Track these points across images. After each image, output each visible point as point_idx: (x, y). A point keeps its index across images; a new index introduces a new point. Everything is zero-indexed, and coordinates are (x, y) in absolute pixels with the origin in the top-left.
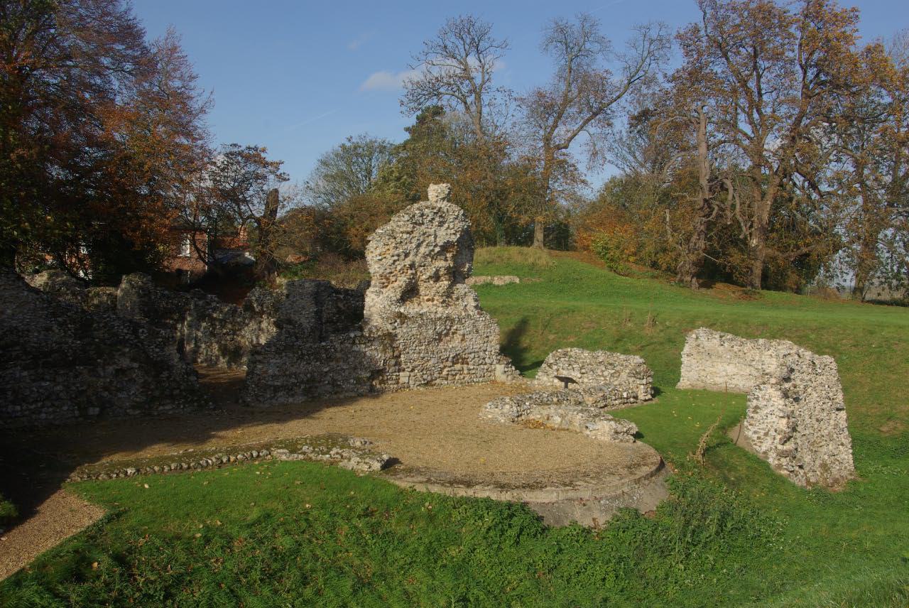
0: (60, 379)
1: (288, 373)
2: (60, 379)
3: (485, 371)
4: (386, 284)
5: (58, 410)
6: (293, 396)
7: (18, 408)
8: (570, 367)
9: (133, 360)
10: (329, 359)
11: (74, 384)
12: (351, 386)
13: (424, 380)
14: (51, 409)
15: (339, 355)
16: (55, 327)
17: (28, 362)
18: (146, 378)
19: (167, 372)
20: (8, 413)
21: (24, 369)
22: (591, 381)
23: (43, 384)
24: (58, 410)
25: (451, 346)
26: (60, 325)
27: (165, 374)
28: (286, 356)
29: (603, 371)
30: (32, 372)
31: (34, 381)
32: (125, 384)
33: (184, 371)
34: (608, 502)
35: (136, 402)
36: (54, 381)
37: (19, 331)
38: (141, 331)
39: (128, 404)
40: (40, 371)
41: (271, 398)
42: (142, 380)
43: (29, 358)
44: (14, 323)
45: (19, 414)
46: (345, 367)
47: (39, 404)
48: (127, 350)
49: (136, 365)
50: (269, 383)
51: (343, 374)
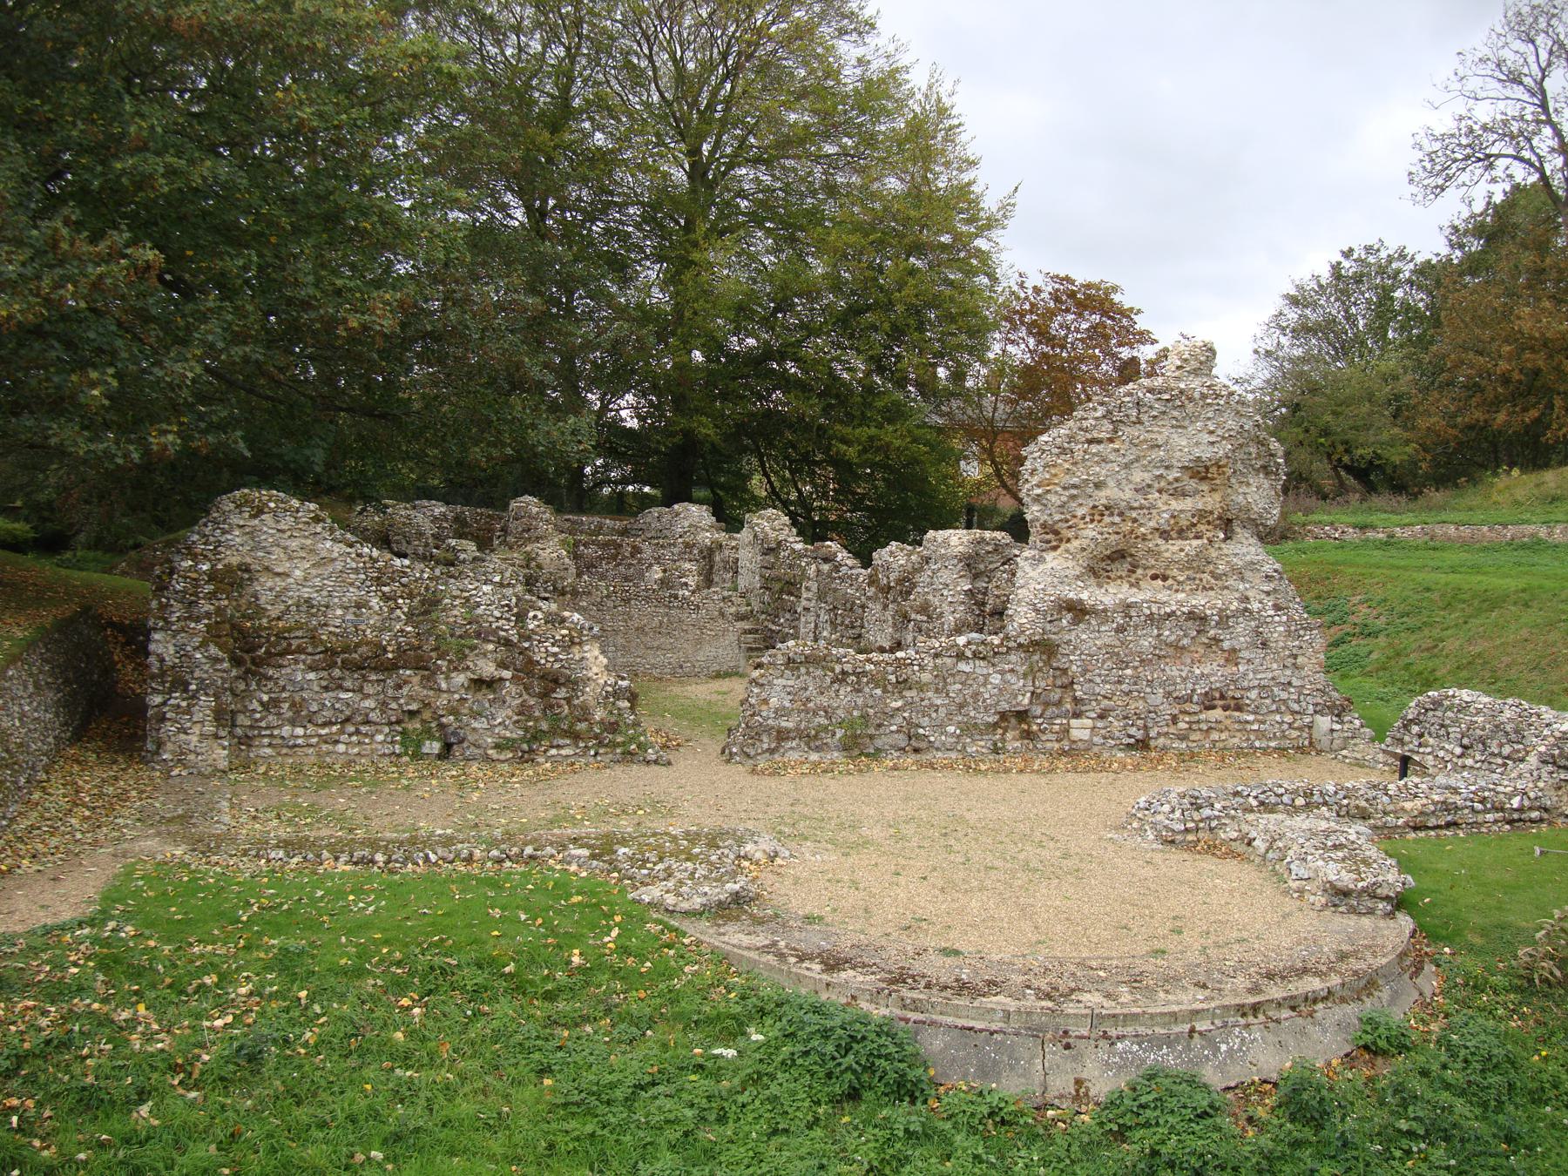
0: (369, 689)
1: (811, 705)
2: (369, 689)
3: (1285, 726)
4: (1054, 543)
5: (367, 741)
6: (818, 749)
7: (300, 731)
8: (1442, 732)
9: (502, 665)
10: (903, 684)
11: (396, 699)
12: (950, 740)
13: (1130, 736)
14: (354, 738)
15: (926, 677)
16: (375, 602)
17: (317, 657)
18: (526, 697)
19: (564, 690)
20: (283, 738)
21: (311, 668)
22: (1478, 765)
23: (343, 695)
24: (367, 741)
25: (1198, 672)
26: (386, 598)
27: (561, 693)
28: (808, 673)
29: (1501, 745)
30: (324, 674)
31: (326, 689)
32: (487, 705)
33: (610, 689)
34: (1135, 1047)
35: (505, 738)
36: (361, 689)
37: (313, 607)
38: (531, 614)
39: (489, 740)
40: (337, 673)
41: (772, 751)
42: (519, 701)
43: (319, 650)
44: (306, 592)
45: (300, 741)
46: (939, 702)
47: (334, 729)
48: (491, 647)
49: (507, 674)
50: (770, 722)
51: (934, 715)
